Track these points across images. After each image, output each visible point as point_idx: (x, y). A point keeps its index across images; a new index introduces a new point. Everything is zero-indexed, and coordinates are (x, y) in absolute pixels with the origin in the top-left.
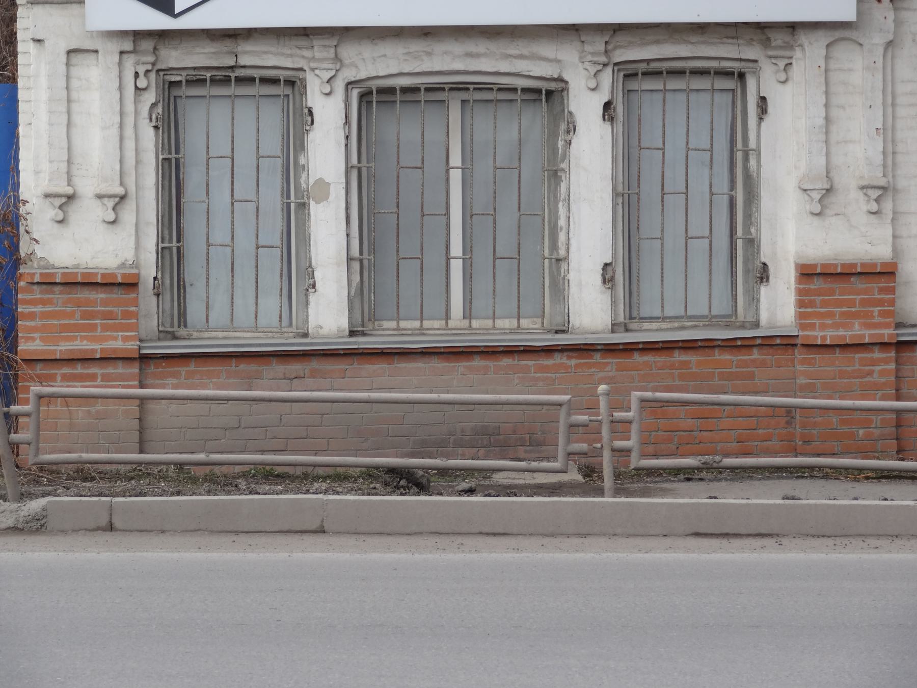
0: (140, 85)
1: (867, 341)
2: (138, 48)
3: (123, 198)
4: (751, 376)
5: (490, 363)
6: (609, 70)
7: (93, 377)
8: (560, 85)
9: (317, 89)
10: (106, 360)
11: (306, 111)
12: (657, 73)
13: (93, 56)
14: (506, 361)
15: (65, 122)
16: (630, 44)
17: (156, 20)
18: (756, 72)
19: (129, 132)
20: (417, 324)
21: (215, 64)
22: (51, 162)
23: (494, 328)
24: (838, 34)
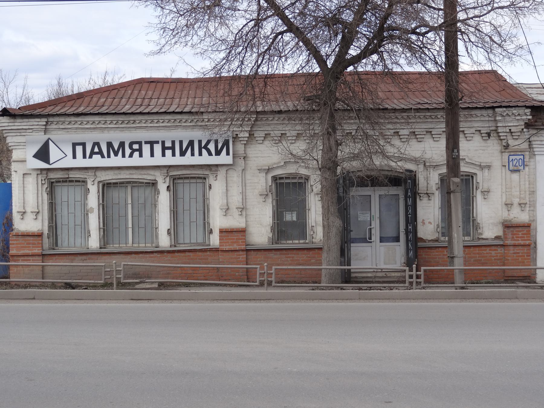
0: (43, 183)
1: (237, 249)
2: (42, 173)
3: (38, 212)
4: (207, 259)
5: (136, 256)
6: (168, 177)
7: (29, 260)
8: (157, 182)
9: (90, 183)
10: (33, 255)
11: (87, 189)
12: (182, 178)
13: (30, 175)
14: (141, 255)
15: (23, 192)
16: (174, 171)
17: (44, 165)
18: (208, 177)
19: (40, 195)
20: (118, 245)
21: (63, 177)
22: (19, 203)
23: (139, 246)
24: (229, 167)
